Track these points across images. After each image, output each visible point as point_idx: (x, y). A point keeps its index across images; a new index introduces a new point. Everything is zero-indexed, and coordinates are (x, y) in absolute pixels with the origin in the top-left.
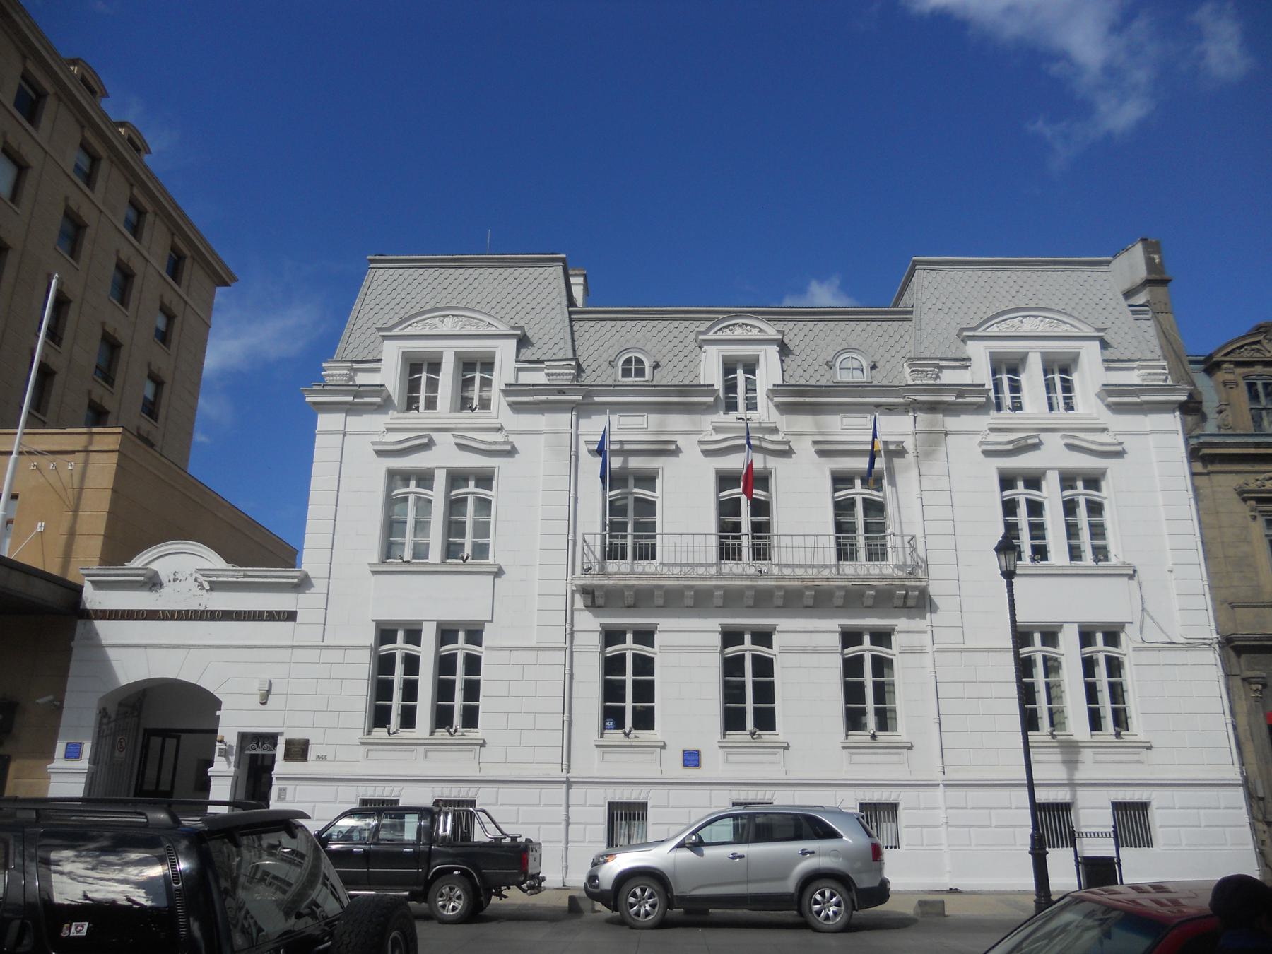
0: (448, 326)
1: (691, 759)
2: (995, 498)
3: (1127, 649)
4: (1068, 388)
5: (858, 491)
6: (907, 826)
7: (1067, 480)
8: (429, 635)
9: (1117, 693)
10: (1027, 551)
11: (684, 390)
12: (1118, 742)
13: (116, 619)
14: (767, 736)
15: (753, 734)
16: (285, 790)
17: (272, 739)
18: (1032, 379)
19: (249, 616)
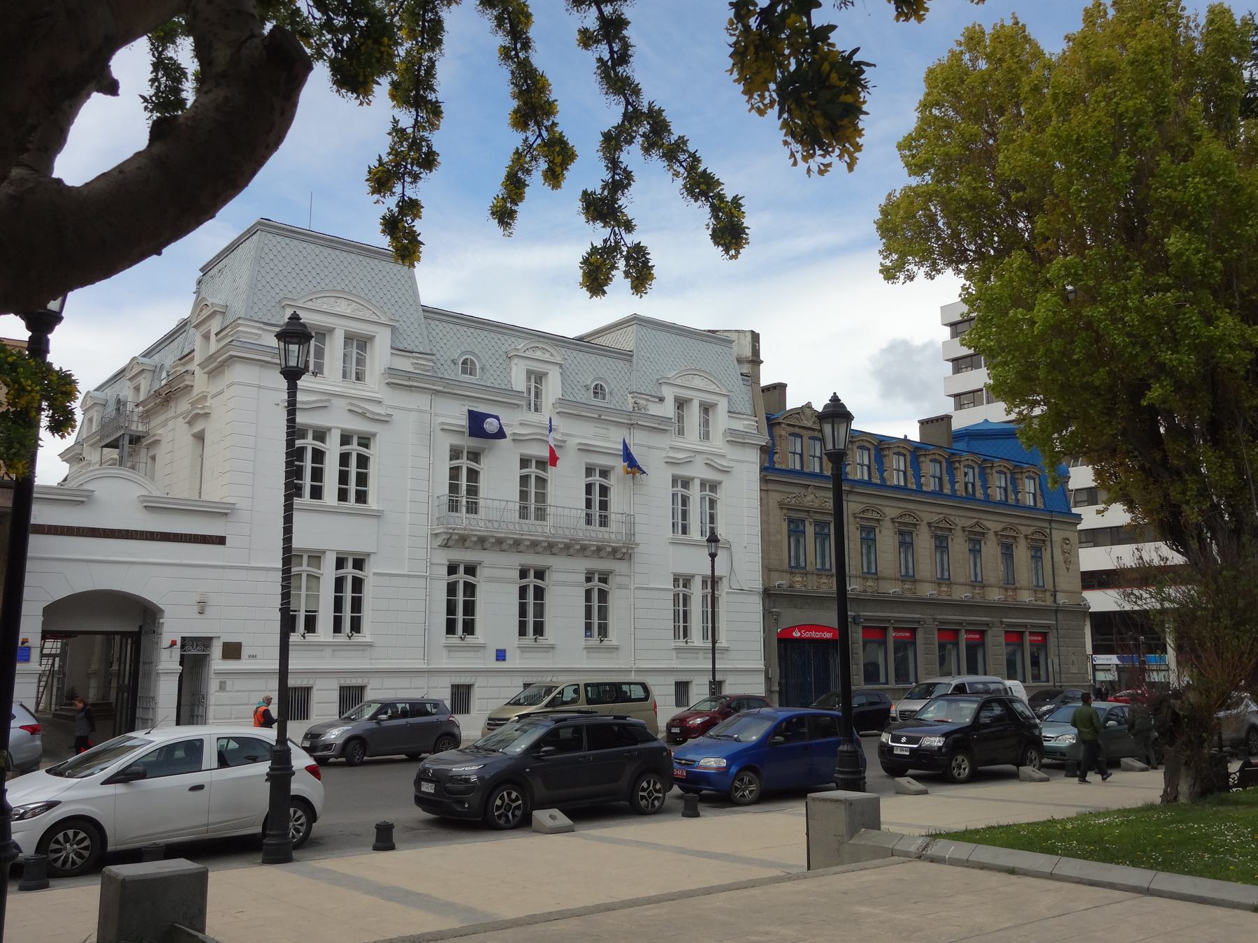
0: (343, 307)
1: (501, 655)
2: (517, 472)
3: (369, 574)
4: (361, 361)
5: (533, 470)
6: (317, 703)
7: (703, 484)
8: (329, 562)
9: (357, 605)
10: (307, 491)
11: (499, 391)
12: (535, 645)
13: (132, 538)
14: (469, 639)
15: (303, 636)
16: (225, 682)
17: (206, 642)
18: (693, 414)
19: (83, 532)
